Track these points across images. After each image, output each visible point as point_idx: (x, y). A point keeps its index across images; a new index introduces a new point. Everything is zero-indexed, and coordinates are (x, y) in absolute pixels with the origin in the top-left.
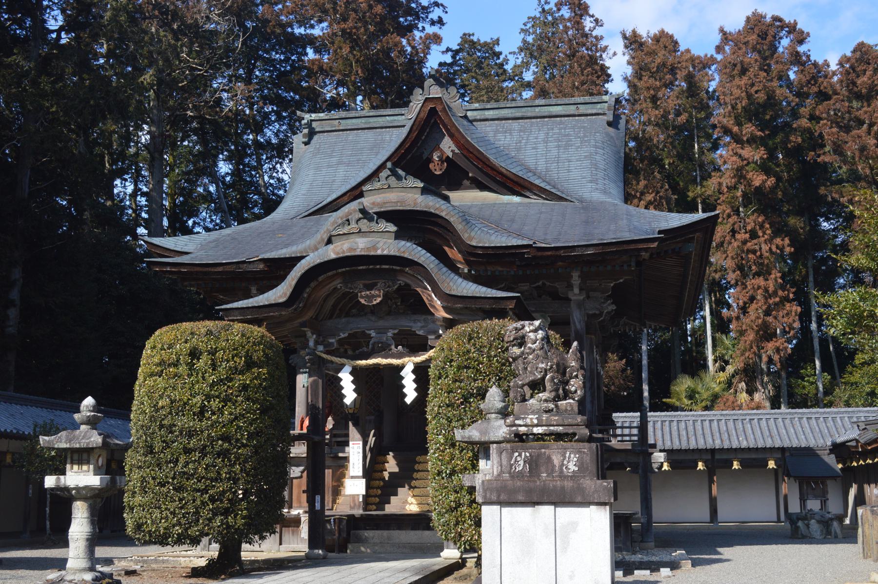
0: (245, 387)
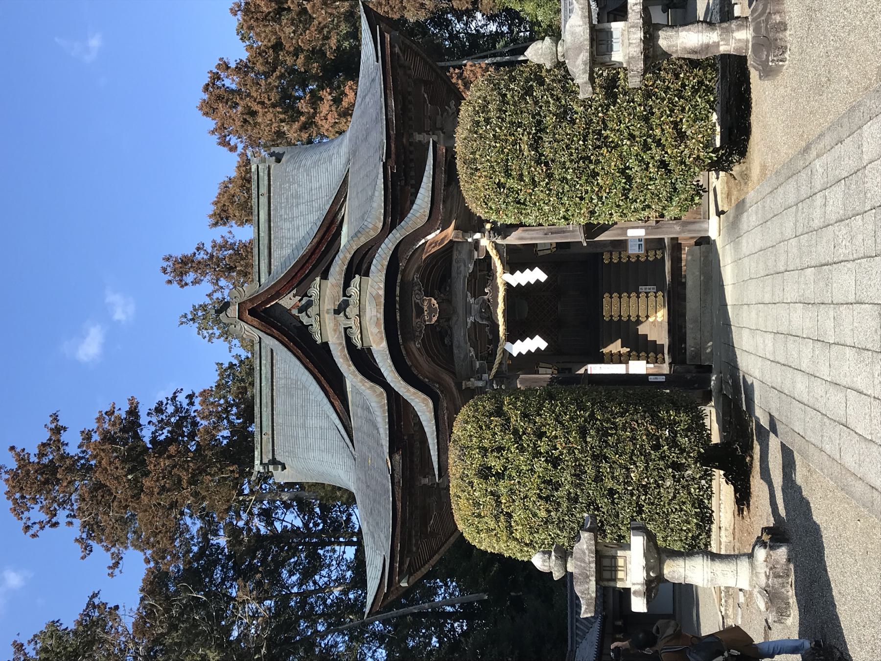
0: (525, 416)
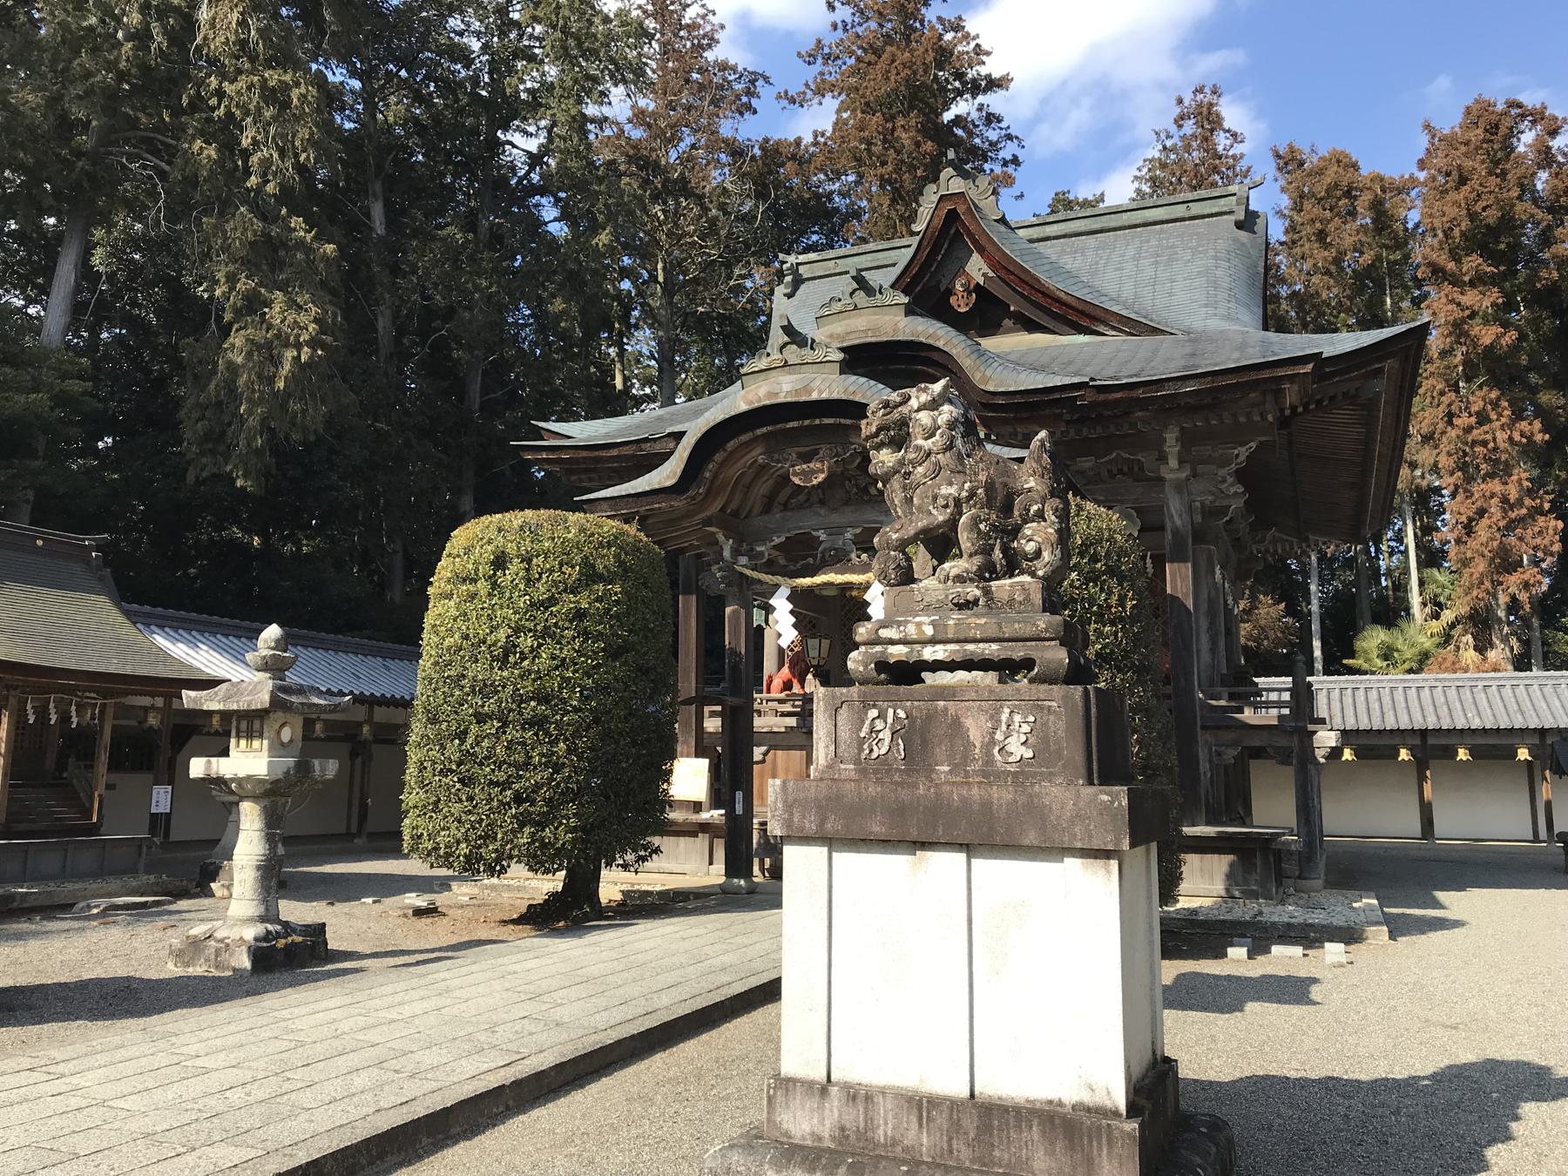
0: (580, 615)
